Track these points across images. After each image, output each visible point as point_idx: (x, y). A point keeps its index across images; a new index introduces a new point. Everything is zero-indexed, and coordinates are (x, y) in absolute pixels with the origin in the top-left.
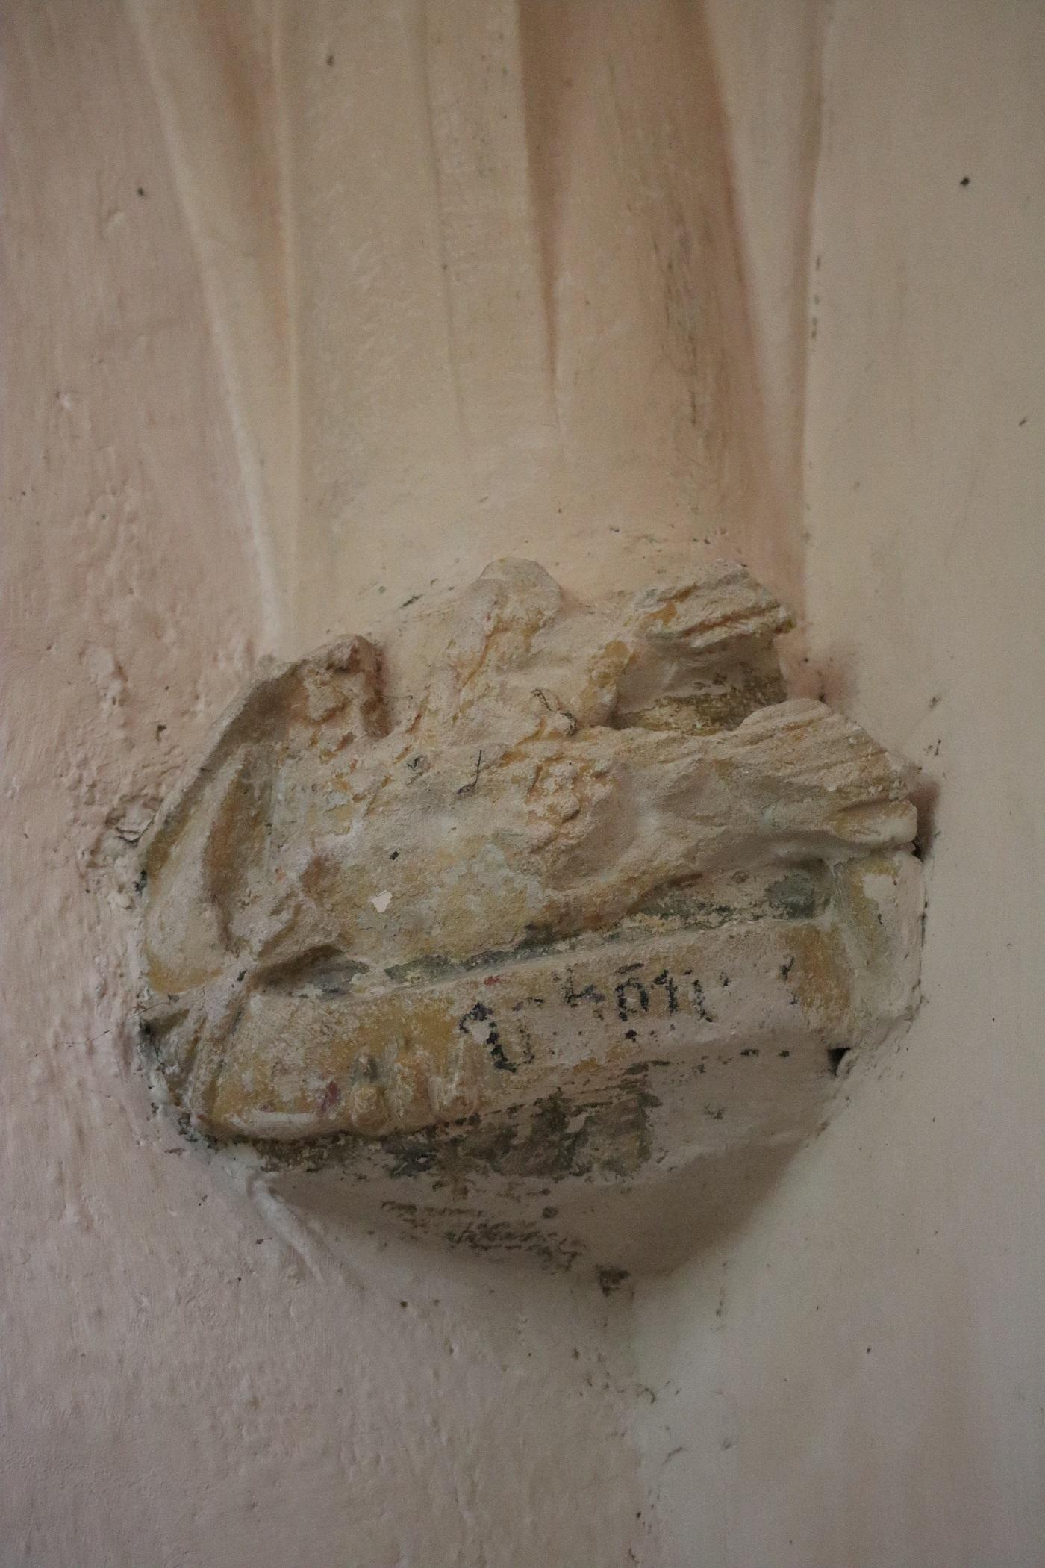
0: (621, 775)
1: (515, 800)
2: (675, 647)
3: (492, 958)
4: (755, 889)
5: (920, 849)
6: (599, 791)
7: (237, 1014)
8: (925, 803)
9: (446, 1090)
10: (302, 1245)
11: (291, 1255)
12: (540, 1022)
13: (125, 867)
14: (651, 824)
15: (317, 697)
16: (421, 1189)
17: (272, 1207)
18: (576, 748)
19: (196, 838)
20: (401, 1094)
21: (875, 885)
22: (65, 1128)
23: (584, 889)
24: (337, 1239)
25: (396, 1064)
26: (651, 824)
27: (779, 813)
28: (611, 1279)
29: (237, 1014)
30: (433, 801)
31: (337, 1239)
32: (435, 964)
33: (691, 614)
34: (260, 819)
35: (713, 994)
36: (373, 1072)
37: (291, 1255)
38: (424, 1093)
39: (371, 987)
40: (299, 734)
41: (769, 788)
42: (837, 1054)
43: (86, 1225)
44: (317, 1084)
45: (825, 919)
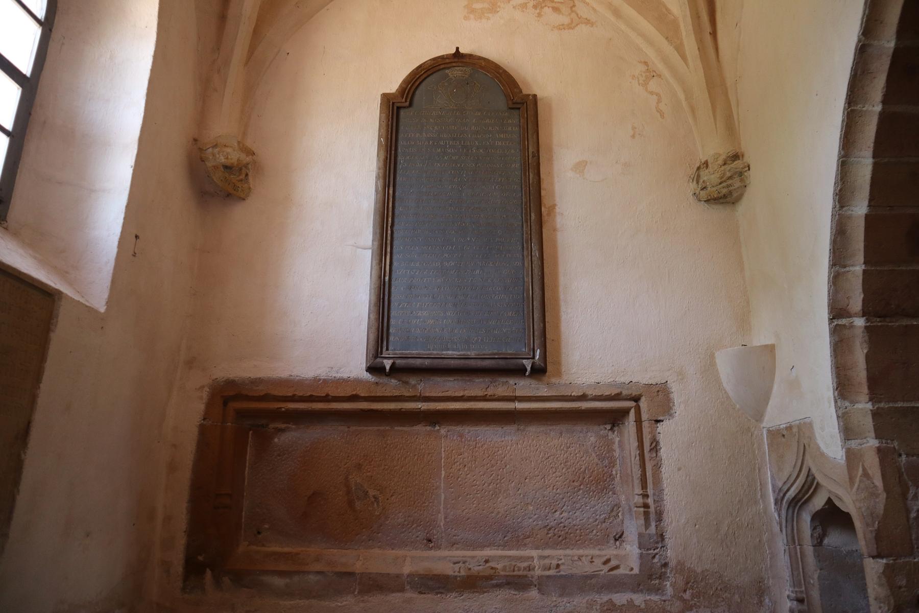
0: (724, 170)
1: (716, 174)
2: (729, 157)
3: (717, 185)
4: (737, 175)
5: (749, 170)
6: (723, 172)
7: (699, 193)
8: (749, 166)
9: (715, 196)
10: (707, 206)
11: (708, 208)
12: (721, 190)
13: (691, 181)
14: (728, 173)
15: (702, 167)
16: (716, 201)
17: (706, 205)
18: (721, 169)
19: (695, 179)
20: (712, 197)
21: (746, 174)
22: (689, 203)
23: (723, 179)
24: (414, 604)
25: (712, 195)
26: (728, 173)
27: (737, 170)
28: (733, 203)
29: (699, 193)
30: (711, 174)
31: (414, 604)
32: (713, 187)
33: (729, 154)
34: (700, 176)
35: (735, 185)
36: (710, 195)
37: (708, 208)
38: (714, 196)
39: (709, 189)
40: (701, 170)
41: (736, 168)
42: (745, 186)
43: (692, 210)
44: (706, 197)
45: (743, 176)
